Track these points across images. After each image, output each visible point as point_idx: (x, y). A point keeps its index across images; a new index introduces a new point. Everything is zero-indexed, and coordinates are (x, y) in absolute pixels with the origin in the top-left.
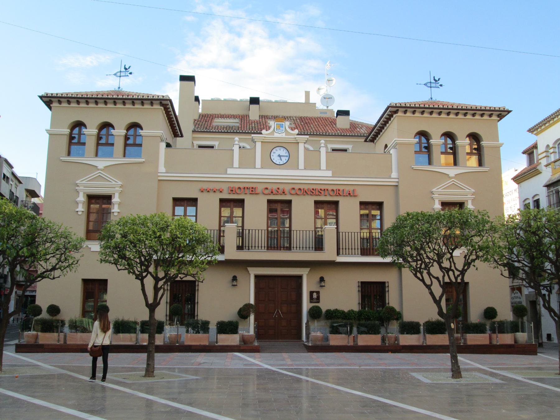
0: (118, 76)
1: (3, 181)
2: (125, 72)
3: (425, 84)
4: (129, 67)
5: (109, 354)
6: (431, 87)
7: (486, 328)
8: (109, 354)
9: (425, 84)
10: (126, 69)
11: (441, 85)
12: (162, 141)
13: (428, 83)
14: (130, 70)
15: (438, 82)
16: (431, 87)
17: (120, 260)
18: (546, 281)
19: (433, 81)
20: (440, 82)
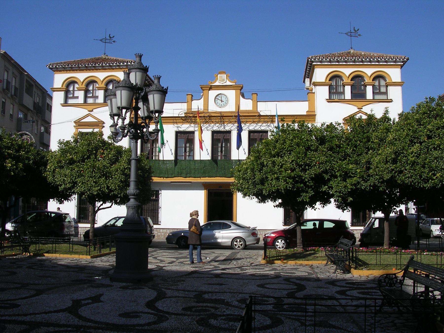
0: (349, 36)
1: (47, 111)
2: (355, 33)
3: (101, 40)
4: (113, 37)
5: (324, 227)
6: (351, 36)
7: (320, 247)
8: (324, 227)
9: (101, 40)
10: (111, 38)
11: (359, 35)
12: (31, 86)
13: (349, 32)
14: (114, 39)
15: (357, 32)
16: (351, 36)
17: (308, 156)
18: (332, 206)
19: (353, 31)
20: (359, 32)
